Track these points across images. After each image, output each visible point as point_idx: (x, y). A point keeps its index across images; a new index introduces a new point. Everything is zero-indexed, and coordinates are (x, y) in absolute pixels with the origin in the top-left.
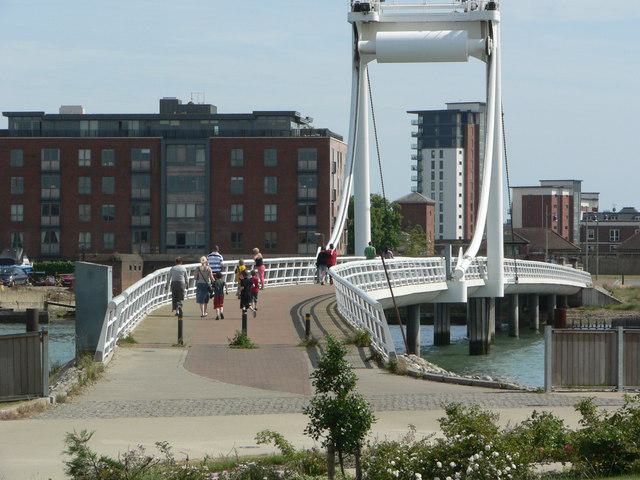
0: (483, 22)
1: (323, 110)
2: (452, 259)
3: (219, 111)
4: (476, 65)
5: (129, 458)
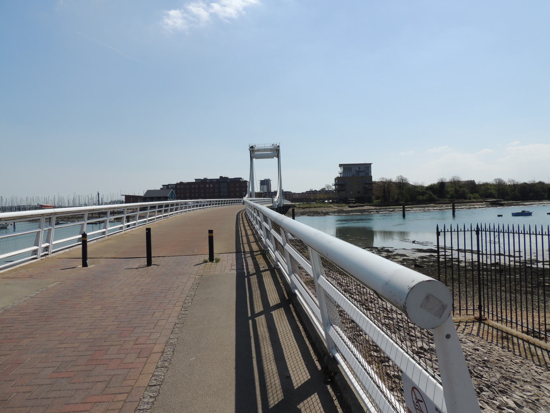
0: (277, 150)
1: (246, 177)
2: (273, 199)
3: (229, 178)
4: (276, 159)
5: (439, 179)
